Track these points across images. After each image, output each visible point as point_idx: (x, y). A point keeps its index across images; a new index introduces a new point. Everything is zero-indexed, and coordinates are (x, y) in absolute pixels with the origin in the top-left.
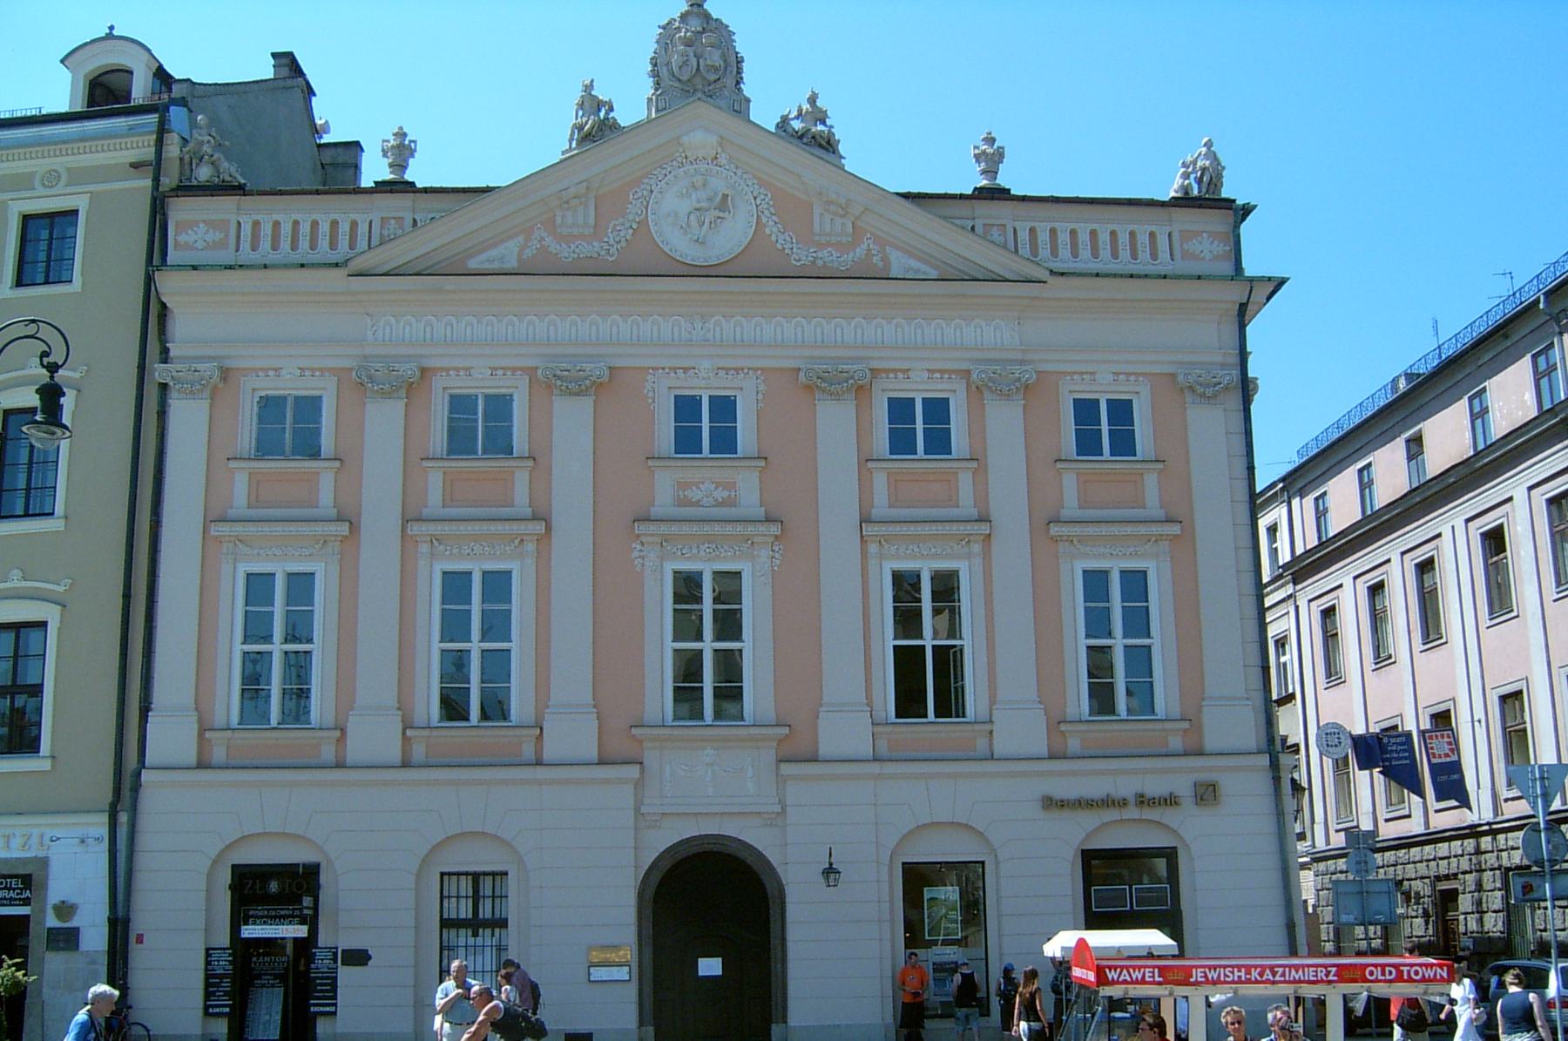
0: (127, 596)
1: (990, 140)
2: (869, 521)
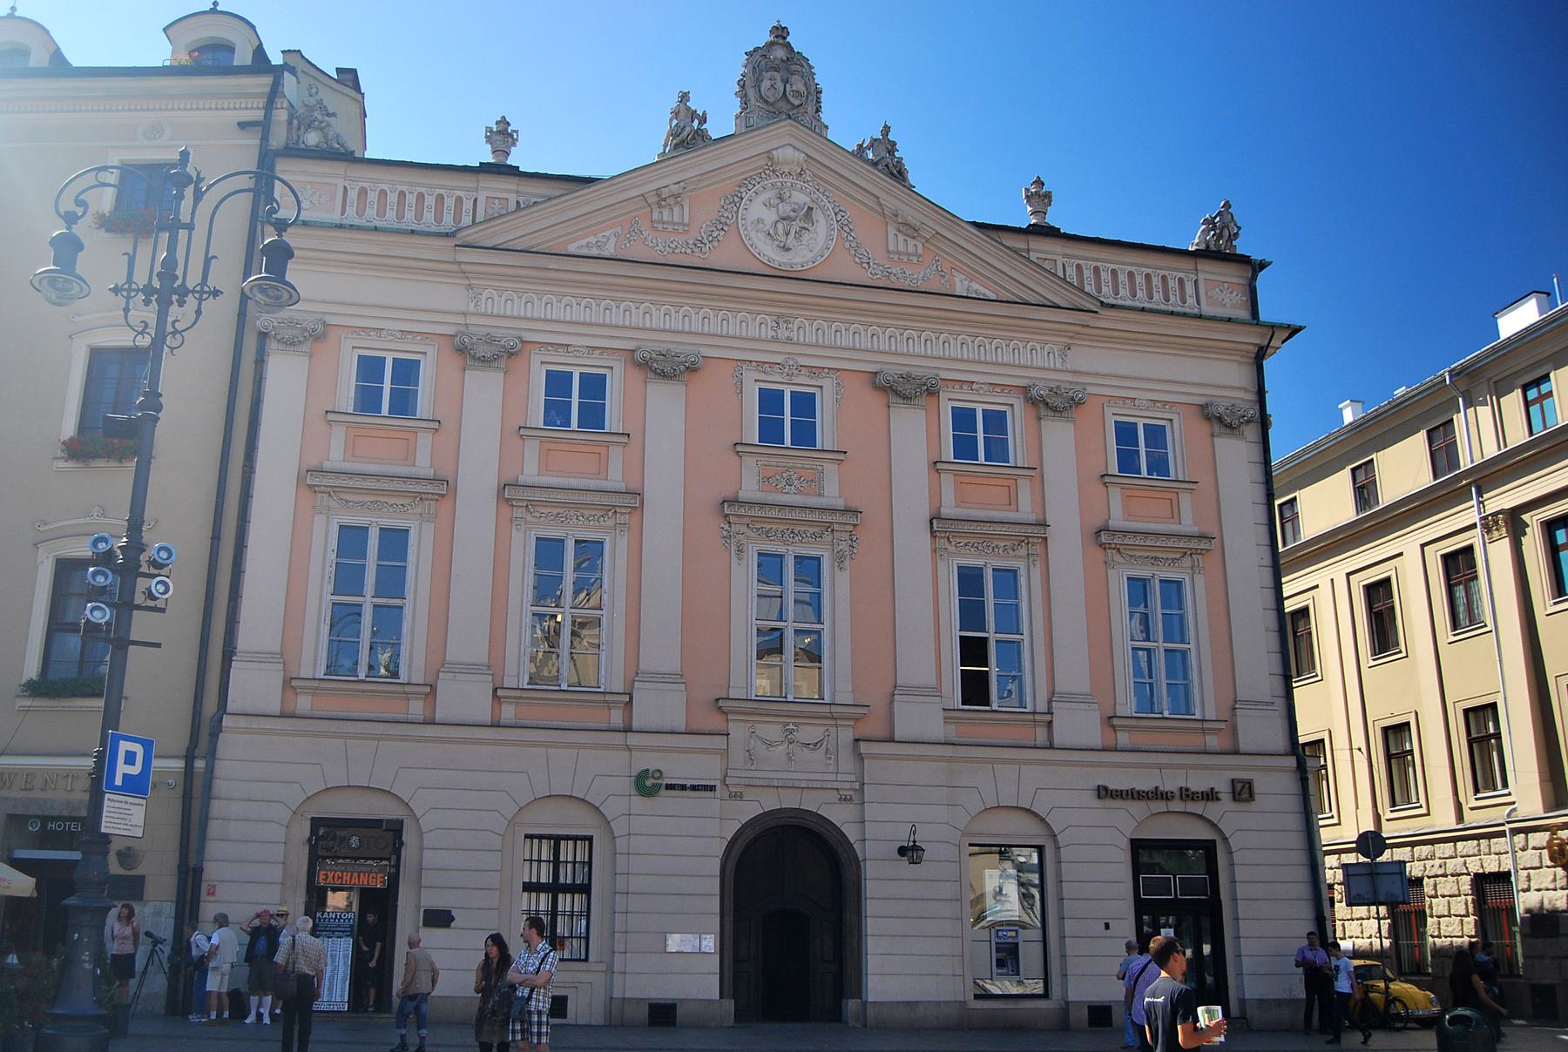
0: (216, 537)
1: (1039, 182)
2: (939, 518)
